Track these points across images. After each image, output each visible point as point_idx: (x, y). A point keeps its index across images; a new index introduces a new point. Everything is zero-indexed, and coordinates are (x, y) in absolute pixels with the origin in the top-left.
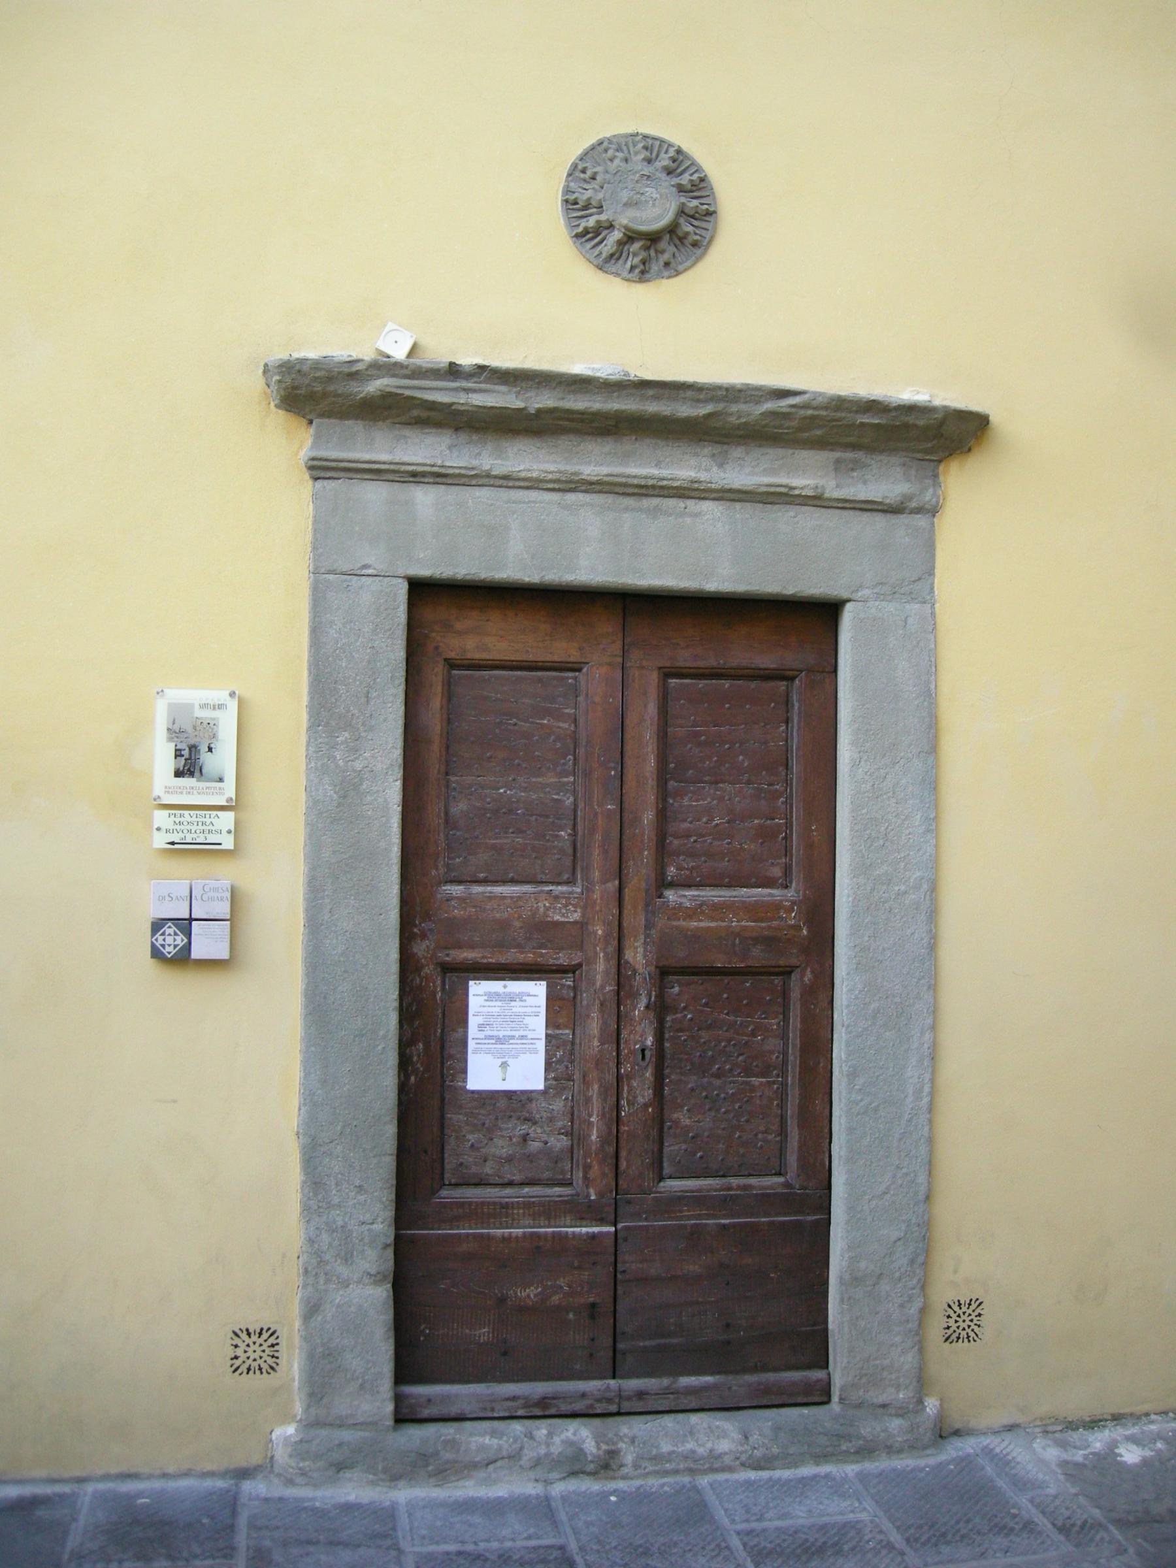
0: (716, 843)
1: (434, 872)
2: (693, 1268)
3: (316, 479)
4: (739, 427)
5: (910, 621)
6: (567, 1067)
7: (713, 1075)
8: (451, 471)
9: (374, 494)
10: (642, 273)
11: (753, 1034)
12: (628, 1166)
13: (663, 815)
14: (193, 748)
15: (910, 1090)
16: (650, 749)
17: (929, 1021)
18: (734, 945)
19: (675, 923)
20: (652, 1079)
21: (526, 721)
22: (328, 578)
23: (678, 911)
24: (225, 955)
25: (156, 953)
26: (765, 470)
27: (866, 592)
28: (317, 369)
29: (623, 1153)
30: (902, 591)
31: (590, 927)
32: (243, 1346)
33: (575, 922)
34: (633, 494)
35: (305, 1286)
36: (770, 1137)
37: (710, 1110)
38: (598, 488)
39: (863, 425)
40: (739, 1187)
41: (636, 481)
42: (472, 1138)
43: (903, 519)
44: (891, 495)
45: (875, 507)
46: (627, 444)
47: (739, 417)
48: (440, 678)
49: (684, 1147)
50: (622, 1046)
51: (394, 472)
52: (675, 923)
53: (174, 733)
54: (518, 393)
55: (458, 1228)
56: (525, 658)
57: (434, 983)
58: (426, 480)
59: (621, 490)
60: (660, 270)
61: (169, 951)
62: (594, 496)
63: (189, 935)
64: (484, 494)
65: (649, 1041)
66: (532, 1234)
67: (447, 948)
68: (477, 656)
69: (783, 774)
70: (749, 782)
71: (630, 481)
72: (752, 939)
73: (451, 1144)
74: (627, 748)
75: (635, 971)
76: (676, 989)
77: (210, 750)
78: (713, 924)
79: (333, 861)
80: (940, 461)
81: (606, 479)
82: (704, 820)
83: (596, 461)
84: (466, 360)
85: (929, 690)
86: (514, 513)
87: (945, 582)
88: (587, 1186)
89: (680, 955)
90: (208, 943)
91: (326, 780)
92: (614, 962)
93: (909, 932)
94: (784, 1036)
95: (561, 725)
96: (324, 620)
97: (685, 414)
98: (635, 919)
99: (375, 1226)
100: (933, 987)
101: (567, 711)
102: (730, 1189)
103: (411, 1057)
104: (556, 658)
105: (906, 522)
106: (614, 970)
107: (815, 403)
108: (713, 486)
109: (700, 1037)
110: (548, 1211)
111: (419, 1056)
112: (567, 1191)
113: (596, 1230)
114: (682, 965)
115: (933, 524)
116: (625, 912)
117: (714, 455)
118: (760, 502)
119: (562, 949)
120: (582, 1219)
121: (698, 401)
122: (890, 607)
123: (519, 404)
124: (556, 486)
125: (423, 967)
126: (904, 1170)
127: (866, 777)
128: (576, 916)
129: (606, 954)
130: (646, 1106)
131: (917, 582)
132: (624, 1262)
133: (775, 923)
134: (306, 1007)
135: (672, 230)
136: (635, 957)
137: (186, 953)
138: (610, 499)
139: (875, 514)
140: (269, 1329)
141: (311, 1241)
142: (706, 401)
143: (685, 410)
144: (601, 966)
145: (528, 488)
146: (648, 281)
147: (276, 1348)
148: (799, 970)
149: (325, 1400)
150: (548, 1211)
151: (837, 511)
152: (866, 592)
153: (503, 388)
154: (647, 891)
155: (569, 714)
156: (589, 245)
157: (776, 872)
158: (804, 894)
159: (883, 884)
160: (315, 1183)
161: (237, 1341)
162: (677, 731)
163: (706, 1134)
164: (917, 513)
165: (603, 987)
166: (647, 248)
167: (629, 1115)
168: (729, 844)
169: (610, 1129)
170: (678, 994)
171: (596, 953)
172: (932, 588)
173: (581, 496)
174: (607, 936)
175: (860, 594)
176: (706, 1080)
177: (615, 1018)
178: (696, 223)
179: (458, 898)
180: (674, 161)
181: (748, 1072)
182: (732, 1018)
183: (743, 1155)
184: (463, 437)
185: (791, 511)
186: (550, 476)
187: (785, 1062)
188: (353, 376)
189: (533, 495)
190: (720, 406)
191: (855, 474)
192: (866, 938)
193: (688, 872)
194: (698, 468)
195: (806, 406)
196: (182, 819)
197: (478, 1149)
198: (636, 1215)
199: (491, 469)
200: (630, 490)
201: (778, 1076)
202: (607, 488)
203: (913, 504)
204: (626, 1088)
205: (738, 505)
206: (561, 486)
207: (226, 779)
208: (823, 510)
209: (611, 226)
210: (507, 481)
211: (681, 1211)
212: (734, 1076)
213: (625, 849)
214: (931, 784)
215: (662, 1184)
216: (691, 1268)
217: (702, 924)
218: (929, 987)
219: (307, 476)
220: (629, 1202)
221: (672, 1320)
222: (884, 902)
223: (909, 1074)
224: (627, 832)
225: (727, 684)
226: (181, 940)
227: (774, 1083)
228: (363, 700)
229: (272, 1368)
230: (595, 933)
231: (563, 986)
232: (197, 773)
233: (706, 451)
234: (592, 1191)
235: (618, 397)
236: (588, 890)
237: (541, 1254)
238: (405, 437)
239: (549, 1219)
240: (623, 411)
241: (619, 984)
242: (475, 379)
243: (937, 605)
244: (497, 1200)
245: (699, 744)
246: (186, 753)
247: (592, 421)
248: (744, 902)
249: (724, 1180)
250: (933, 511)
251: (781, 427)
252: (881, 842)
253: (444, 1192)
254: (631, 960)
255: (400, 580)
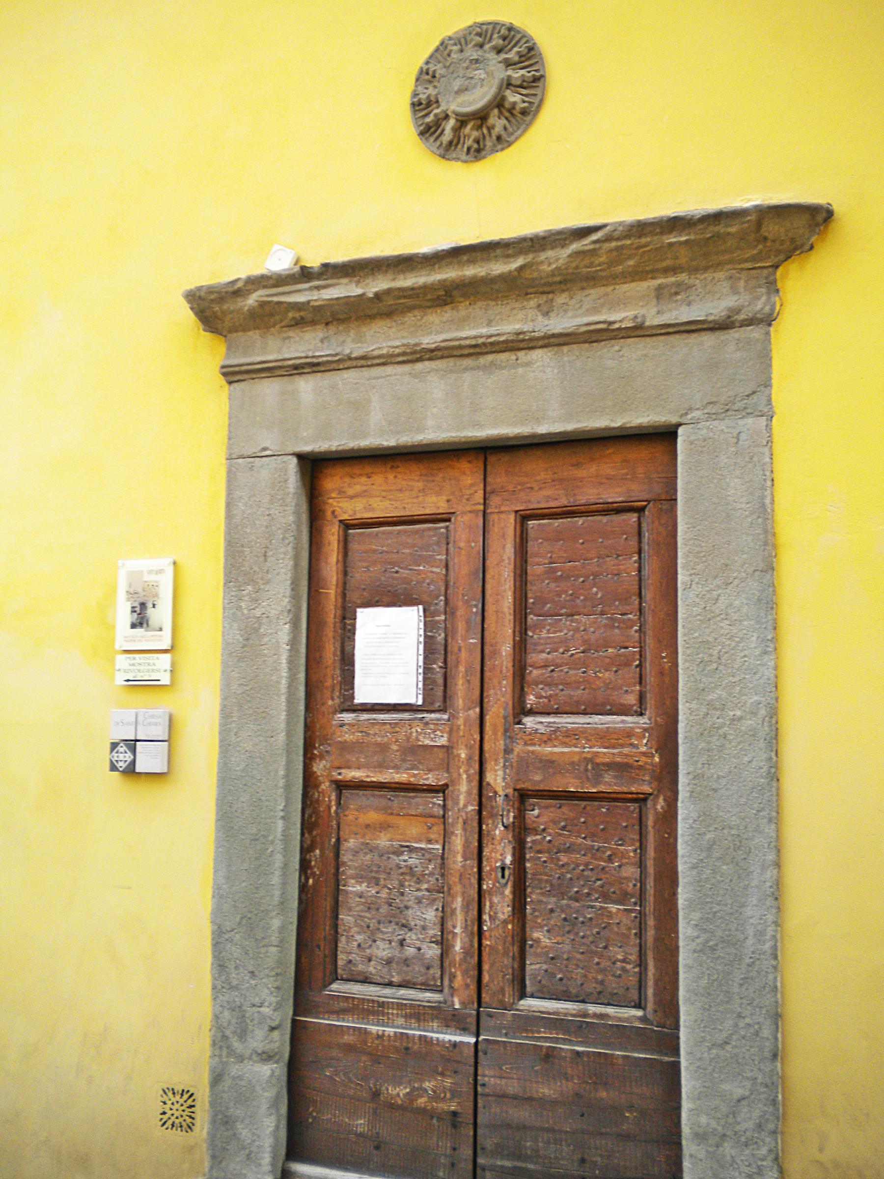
0: (572, 672)
1: (330, 703)
2: (546, 1091)
3: (230, 383)
4: (553, 274)
5: (743, 437)
6: (437, 880)
7: (571, 898)
8: (320, 360)
9: (269, 390)
10: (477, 152)
11: (610, 859)
12: (492, 980)
13: (521, 646)
14: (143, 605)
15: (751, 931)
16: (507, 587)
17: (771, 857)
18: (586, 770)
19: (531, 748)
20: (511, 897)
21: (406, 569)
22: (240, 459)
23: (533, 737)
24: (165, 771)
25: (113, 768)
26: (587, 310)
27: (696, 414)
28: (211, 293)
29: (486, 967)
30: (736, 407)
31: (455, 751)
32: (169, 1103)
33: (442, 746)
34: (469, 355)
35: (213, 1056)
36: (629, 967)
37: (569, 932)
38: (439, 354)
39: (671, 245)
40: (595, 1015)
41: (468, 342)
42: (359, 938)
43: (733, 334)
44: (714, 311)
45: (700, 326)
46: (463, 309)
47: (550, 264)
48: (336, 537)
49: (545, 967)
50: (485, 863)
51: (280, 367)
52: (531, 748)
53: (131, 594)
54: (359, 282)
55: (343, 1020)
56: (402, 513)
57: (329, 797)
58: (305, 371)
59: (459, 353)
60: (494, 145)
61: (122, 765)
62: (438, 362)
63: (134, 751)
64: (350, 376)
65: (508, 860)
66: (402, 1033)
67: (340, 768)
68: (366, 515)
69: (637, 602)
70: (602, 613)
71: (463, 343)
72: (604, 764)
73: (342, 942)
74: (488, 587)
75: (496, 793)
76: (536, 812)
77: (154, 606)
78: (566, 750)
79: (239, 692)
80: (776, 267)
81: (443, 344)
82: (561, 650)
83: (435, 329)
84: (314, 261)
85: (763, 506)
86: (374, 387)
87: (782, 393)
88: (452, 996)
89: (536, 779)
90: (149, 759)
91: (235, 625)
92: (475, 783)
93: (746, 759)
94: (641, 865)
95: (435, 570)
96: (235, 496)
97: (499, 272)
98: (495, 743)
99: (262, 1009)
100: (776, 818)
101: (439, 557)
102: (585, 1015)
103: (310, 861)
104: (428, 512)
105: (737, 335)
106: (475, 791)
107: (616, 234)
108: (536, 334)
109: (559, 860)
110: (417, 1014)
111: (316, 861)
112: (437, 997)
113: (458, 1039)
114: (537, 788)
115: (768, 333)
116: (486, 737)
117: (539, 306)
118: (585, 342)
119: (430, 770)
120: (447, 1026)
121: (508, 256)
122: (720, 425)
123: (359, 291)
124: (404, 358)
125: (320, 783)
126: (747, 1020)
127: (697, 600)
128: (443, 741)
129: (468, 776)
130: (505, 922)
131: (754, 397)
132: (484, 1076)
133: (626, 750)
134: (217, 814)
135: (499, 103)
136: (495, 780)
137: (132, 767)
138: (451, 362)
139: (703, 333)
140: (188, 1091)
141: (216, 1017)
142: (515, 256)
143: (498, 268)
144: (463, 787)
145: (383, 364)
146: (484, 157)
147: (193, 1109)
148: (651, 797)
149: (224, 1163)
150: (417, 1014)
151: (663, 338)
152: (696, 414)
153: (345, 281)
154: (505, 718)
155: (441, 560)
156: (432, 139)
157: (631, 699)
158: (656, 721)
159: (716, 709)
160: (220, 966)
161: (165, 1098)
162: (535, 569)
163: (565, 956)
164: (748, 325)
165: (465, 806)
166: (479, 127)
167: (490, 929)
168: (584, 672)
169: (471, 941)
170: (538, 817)
171: (459, 775)
172: (769, 400)
173: (427, 363)
174: (470, 758)
175: (689, 416)
176: (565, 902)
177: (476, 836)
178: (524, 92)
179: (348, 724)
180: (504, 39)
181: (605, 897)
182: (589, 842)
183: (602, 983)
184: (332, 329)
185: (616, 345)
186: (397, 351)
187: (642, 892)
188: (237, 293)
189: (389, 369)
190: (530, 257)
191: (679, 297)
192: (700, 766)
193: (546, 700)
194: (525, 320)
195: (608, 239)
196: (134, 662)
197: (364, 949)
198: (497, 1030)
199: (351, 353)
200: (466, 352)
201: (635, 904)
202: (446, 353)
203: (742, 317)
204: (488, 904)
205: (565, 349)
206: (409, 358)
207: (164, 629)
208: (648, 339)
209: (447, 117)
210: (366, 361)
211: (539, 1032)
212: (591, 901)
213: (486, 680)
214: (769, 602)
215: (522, 1002)
216: (546, 1091)
217: (556, 750)
218: (770, 820)
219: (222, 381)
220: (490, 1015)
221: (528, 1144)
222: (718, 728)
223: (749, 913)
224: (488, 663)
225: (580, 521)
226: (129, 757)
227: (631, 911)
228: (262, 559)
229: (189, 1127)
230: (459, 756)
231: (434, 804)
232: (145, 625)
233: (533, 303)
234: (456, 1000)
235: (439, 268)
236: (452, 717)
237: (411, 1057)
238: (289, 337)
239: (419, 1020)
240: (445, 280)
241: (480, 804)
242: (325, 277)
243: (774, 419)
244: (376, 998)
245: (556, 579)
246: (138, 609)
247: (425, 295)
248: (596, 729)
249: (582, 1006)
250: (768, 320)
251: (591, 265)
252: (715, 666)
253: (334, 986)
254: (492, 782)
255: (290, 457)
